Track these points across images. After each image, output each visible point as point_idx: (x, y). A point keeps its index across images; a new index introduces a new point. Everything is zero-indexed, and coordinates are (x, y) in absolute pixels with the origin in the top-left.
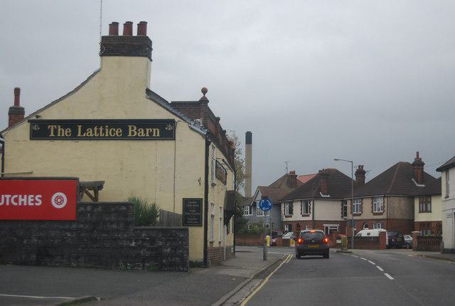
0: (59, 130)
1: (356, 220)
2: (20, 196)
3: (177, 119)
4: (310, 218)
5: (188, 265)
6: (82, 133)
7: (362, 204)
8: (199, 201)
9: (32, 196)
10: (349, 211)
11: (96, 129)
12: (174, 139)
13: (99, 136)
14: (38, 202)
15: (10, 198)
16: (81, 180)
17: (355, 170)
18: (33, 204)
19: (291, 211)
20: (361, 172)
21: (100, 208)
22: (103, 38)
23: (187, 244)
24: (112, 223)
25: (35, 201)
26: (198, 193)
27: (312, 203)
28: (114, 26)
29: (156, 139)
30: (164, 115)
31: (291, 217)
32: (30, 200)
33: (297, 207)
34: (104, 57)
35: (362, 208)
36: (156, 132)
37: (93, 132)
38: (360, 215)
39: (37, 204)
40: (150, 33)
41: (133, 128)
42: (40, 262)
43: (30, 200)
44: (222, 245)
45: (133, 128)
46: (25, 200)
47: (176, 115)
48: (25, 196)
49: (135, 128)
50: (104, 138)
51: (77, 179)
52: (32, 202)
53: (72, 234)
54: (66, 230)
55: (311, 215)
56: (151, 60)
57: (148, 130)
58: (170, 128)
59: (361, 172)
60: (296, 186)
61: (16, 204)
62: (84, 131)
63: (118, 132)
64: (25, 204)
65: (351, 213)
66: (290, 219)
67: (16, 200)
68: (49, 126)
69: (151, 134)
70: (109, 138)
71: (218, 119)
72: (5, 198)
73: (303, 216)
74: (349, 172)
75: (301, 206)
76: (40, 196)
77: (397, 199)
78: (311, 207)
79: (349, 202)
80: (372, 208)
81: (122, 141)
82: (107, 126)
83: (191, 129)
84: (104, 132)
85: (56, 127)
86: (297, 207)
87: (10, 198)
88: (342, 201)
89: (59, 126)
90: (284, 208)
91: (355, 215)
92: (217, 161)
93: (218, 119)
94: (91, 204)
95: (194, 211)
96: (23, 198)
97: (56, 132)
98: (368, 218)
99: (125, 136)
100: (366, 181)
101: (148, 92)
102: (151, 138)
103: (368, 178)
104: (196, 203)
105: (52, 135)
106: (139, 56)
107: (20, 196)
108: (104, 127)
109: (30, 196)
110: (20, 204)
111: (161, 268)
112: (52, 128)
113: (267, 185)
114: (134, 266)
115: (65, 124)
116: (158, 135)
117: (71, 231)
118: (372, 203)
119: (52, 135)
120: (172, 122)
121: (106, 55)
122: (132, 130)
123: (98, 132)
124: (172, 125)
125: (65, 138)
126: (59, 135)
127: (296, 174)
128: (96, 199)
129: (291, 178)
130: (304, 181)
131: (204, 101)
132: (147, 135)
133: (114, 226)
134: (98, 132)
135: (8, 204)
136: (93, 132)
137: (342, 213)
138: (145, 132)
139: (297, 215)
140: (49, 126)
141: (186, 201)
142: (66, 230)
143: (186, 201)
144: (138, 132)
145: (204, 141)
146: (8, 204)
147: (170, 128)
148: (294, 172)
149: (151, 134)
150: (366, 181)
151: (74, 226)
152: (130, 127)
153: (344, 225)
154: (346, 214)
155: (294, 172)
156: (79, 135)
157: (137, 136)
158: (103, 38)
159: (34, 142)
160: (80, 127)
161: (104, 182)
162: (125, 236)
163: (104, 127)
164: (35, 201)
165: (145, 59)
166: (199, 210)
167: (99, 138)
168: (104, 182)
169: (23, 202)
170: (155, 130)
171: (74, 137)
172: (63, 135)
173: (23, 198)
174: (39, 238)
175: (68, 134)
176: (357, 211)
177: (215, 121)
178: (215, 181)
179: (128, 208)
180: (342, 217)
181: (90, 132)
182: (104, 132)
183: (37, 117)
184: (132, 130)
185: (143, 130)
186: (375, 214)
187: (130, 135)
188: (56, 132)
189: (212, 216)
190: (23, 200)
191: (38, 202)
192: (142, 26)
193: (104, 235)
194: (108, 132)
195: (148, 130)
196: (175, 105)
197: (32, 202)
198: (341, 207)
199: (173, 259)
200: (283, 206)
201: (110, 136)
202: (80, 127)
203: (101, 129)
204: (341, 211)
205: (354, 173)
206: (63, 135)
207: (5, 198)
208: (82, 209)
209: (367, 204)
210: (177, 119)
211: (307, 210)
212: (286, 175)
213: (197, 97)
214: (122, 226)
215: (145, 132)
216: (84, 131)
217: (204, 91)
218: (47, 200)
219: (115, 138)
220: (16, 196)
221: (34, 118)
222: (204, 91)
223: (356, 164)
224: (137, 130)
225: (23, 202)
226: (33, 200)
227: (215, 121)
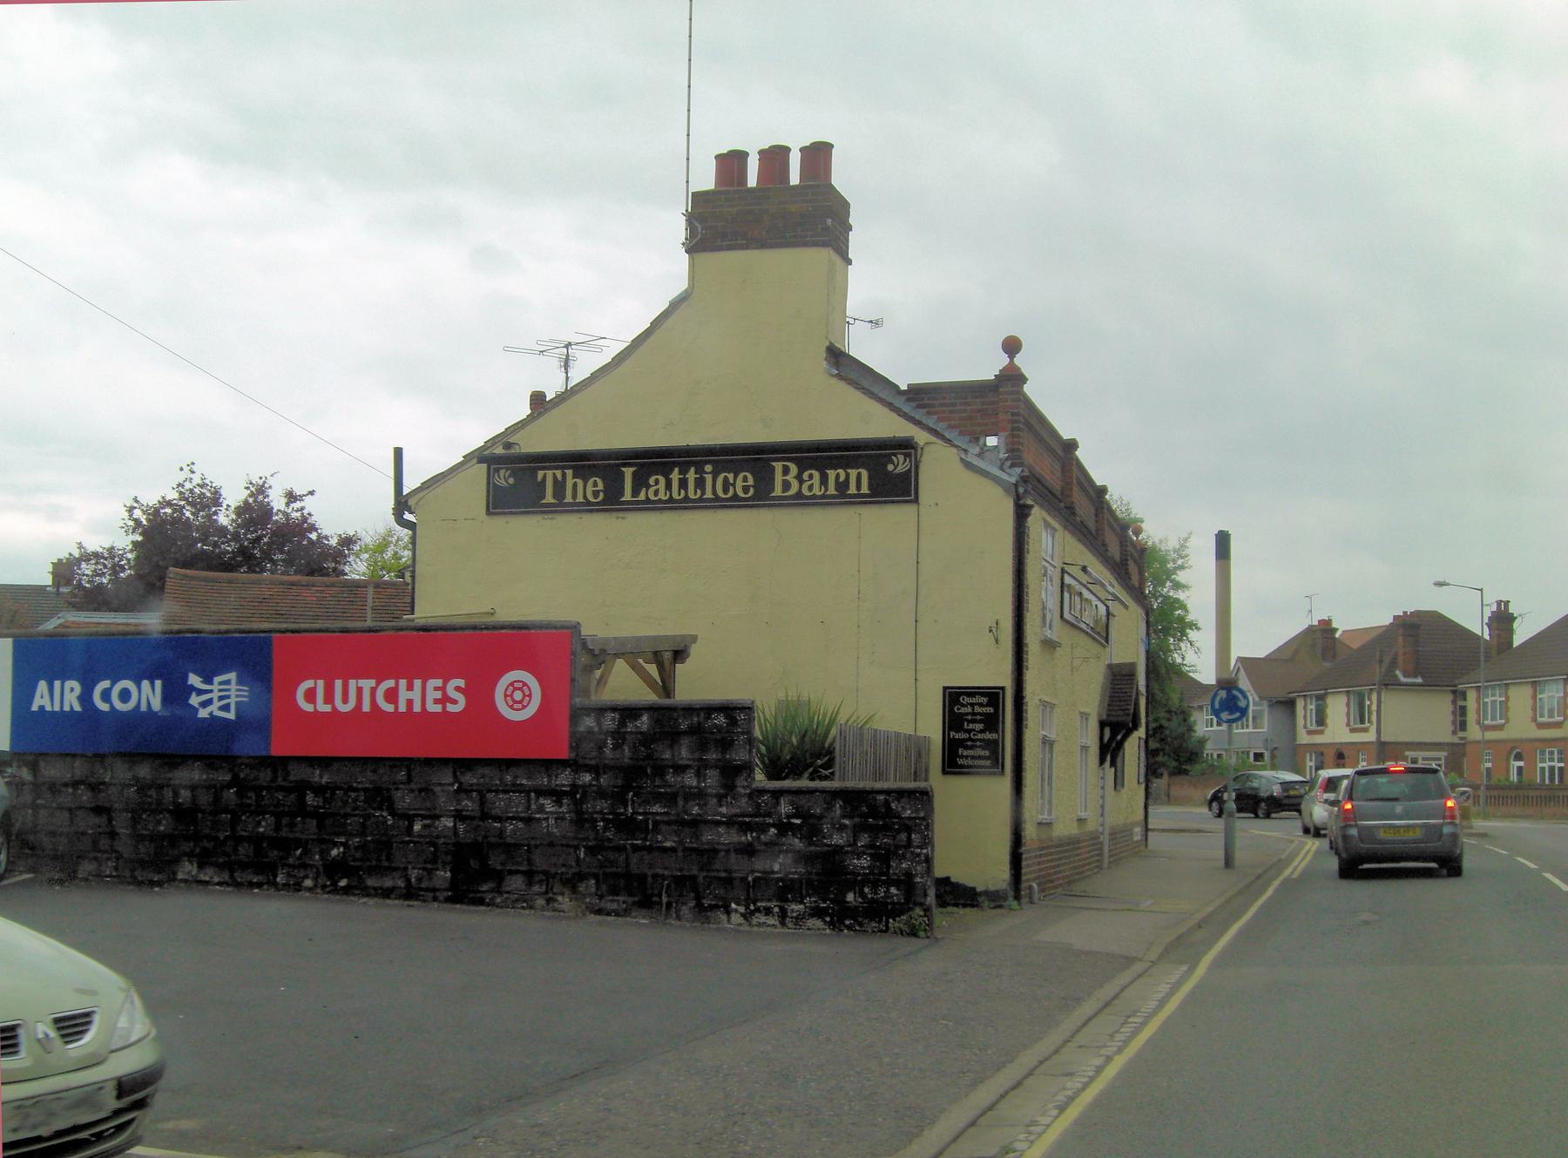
0: (570, 482)
1: (1488, 742)
2: (403, 683)
3: (921, 437)
4: (1371, 736)
5: (931, 899)
6: (635, 493)
7: (1507, 699)
8: (993, 696)
9: (439, 683)
10: (1471, 717)
11: (675, 476)
12: (916, 501)
13: (671, 500)
14: (454, 702)
15: (373, 691)
16: (586, 631)
17: (1487, 614)
18: (438, 708)
19: (1321, 720)
20: (1502, 619)
21: (645, 718)
22: (699, 198)
23: (927, 842)
24: (680, 769)
25: (445, 700)
26: (994, 672)
27: (1374, 697)
28: (731, 163)
29: (860, 500)
30: (881, 424)
31: (1322, 732)
32: (432, 695)
33: (1338, 708)
34: (704, 258)
35: (1507, 709)
36: (858, 479)
37: (669, 486)
38: (1499, 728)
39: (451, 708)
40: (841, 178)
41: (786, 471)
42: (463, 893)
43: (432, 695)
44: (1091, 826)
45: (786, 471)
46: (416, 695)
47: (918, 423)
48: (418, 683)
49: (794, 469)
50: (701, 504)
51: (575, 627)
52: (436, 701)
53: (559, 803)
54: (541, 793)
55: (1373, 729)
56: (849, 262)
57: (832, 474)
58: (899, 465)
59: (1502, 619)
60: (1334, 657)
61: (389, 708)
62: (640, 482)
63: (743, 482)
64: (417, 708)
65: (1478, 722)
66: (1318, 739)
67: (392, 696)
68: (540, 474)
69: (842, 487)
70: (717, 504)
71: (1071, 446)
72: (360, 690)
73: (1353, 730)
74: (1474, 621)
75: (1348, 705)
76: (461, 683)
77: (1223, 827)
78: (1374, 708)
79: (1472, 696)
80: (1534, 709)
81: (754, 512)
82: (708, 468)
83: (968, 466)
84: (700, 483)
85: (559, 473)
86: (1338, 708)
87: (373, 691)
88: (1454, 692)
89: (569, 472)
90: (1304, 710)
91: (1541, 726)
92: (1063, 571)
93: (1071, 446)
94: (652, 709)
95: (979, 726)
96: (410, 687)
97: (559, 487)
98: (1525, 736)
99: (762, 496)
100: (1518, 640)
101: (837, 357)
102: (843, 497)
103: (1522, 633)
104: (984, 700)
105: (549, 499)
106: (805, 245)
107: (403, 683)
108: (700, 471)
109: (434, 683)
110: (402, 708)
111: (840, 918)
112: (548, 476)
113: (1261, 654)
114: (752, 913)
115: (582, 463)
116: (865, 490)
117: (557, 795)
118: (1534, 697)
119: (549, 499)
120: (905, 446)
121: (704, 250)
122: (783, 475)
123: (683, 484)
124: (907, 455)
125: (588, 507)
126: (569, 499)
127: (1334, 625)
128: (667, 689)
129: (1321, 636)
130: (1355, 645)
131: (1012, 378)
132: (832, 490)
133: (690, 780)
134: (683, 484)
135: (366, 708)
136: (669, 486)
137: (1454, 723)
138: (824, 480)
139: (1338, 730)
140: (540, 474)
141: (953, 696)
142: (541, 793)
143: (953, 696)
144: (801, 482)
145: (1007, 507)
146: (366, 708)
147: (899, 465)
148: (1328, 622)
149: (842, 487)
150: (1518, 640)
151: (564, 779)
152: (778, 466)
153: (1457, 754)
154: (1463, 726)
155: (1328, 622)
156: (628, 496)
157: (799, 495)
158: (699, 198)
159: (499, 522)
160: (628, 472)
161: (694, 639)
162: (724, 810)
163: (700, 471)
164: (445, 700)
165: (824, 255)
166: (992, 722)
167: (685, 505)
168: (694, 639)
169: (410, 703)
170: (853, 473)
171: (612, 501)
172: (580, 499)
173: (410, 687)
174: (459, 816)
175: (596, 494)
176: (1493, 718)
177: (1060, 453)
178: (1057, 632)
179: (733, 722)
180: (1454, 732)
181: (657, 487)
182: (700, 483)
183: (508, 446)
184: (783, 475)
185: (816, 474)
186: (1541, 726)
187: (778, 491)
188: (559, 487)
189: (1047, 743)
190: (410, 695)
191: (454, 702)
192: (818, 155)
193: (657, 808)
194: (714, 485)
195: (832, 474)
196: (921, 395)
197: (436, 701)
198: (1451, 708)
199: (882, 892)
200: (1300, 704)
201: (717, 498)
202: (628, 472)
203: (692, 475)
204: (1451, 718)
205: (1486, 620)
206: (580, 499)
207: (360, 690)
208: (589, 722)
209: (1520, 697)
210: (921, 437)
211: (1361, 716)
212: (1310, 630)
213: (986, 368)
214: (712, 780)
215: (824, 480)
216: (640, 482)
217: (1012, 346)
218: (479, 693)
219: (735, 503)
220: (390, 683)
221: (499, 450)
222: (1012, 346)
223: (1491, 599)
224: (799, 477)
225: (410, 703)
226: (439, 695)
227: (1060, 453)
